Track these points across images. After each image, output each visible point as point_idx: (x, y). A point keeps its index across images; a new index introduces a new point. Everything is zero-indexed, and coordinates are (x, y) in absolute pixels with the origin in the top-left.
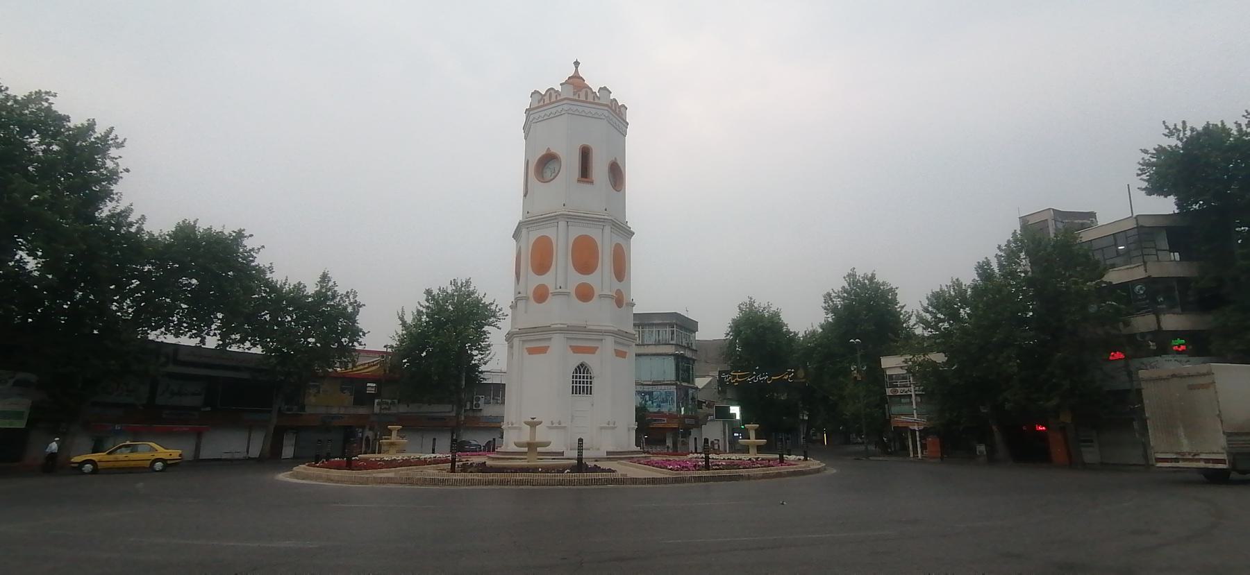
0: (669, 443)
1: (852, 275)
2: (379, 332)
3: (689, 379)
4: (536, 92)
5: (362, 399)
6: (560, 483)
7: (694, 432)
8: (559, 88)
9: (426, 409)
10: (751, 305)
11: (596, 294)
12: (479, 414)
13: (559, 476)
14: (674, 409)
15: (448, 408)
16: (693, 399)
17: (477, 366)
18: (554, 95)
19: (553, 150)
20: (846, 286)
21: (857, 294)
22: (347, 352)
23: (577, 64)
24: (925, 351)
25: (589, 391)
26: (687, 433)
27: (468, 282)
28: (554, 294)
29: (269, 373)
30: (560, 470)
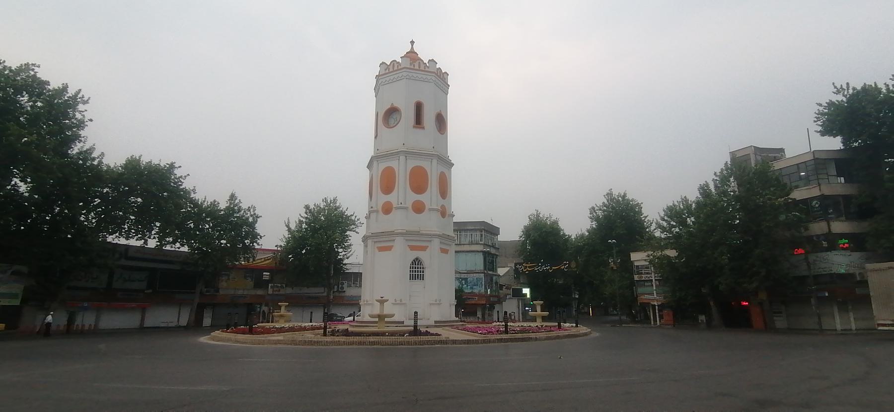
0: (479, 314)
1: (609, 194)
2: (272, 236)
3: (494, 269)
4: (383, 63)
5: (260, 284)
6: (401, 344)
7: (497, 307)
8: (399, 60)
9: (305, 290)
10: (538, 216)
11: (427, 207)
12: (343, 294)
13: (401, 339)
14: (483, 290)
15: (321, 290)
16: (496, 283)
17: (342, 260)
18: (396, 66)
19: (395, 105)
20: (606, 202)
21: (613, 208)
22: (249, 250)
23: (412, 42)
24: (662, 248)
25: (422, 278)
26: (492, 308)
27: (335, 200)
28: (397, 208)
29: (193, 266)
30: (402, 334)
